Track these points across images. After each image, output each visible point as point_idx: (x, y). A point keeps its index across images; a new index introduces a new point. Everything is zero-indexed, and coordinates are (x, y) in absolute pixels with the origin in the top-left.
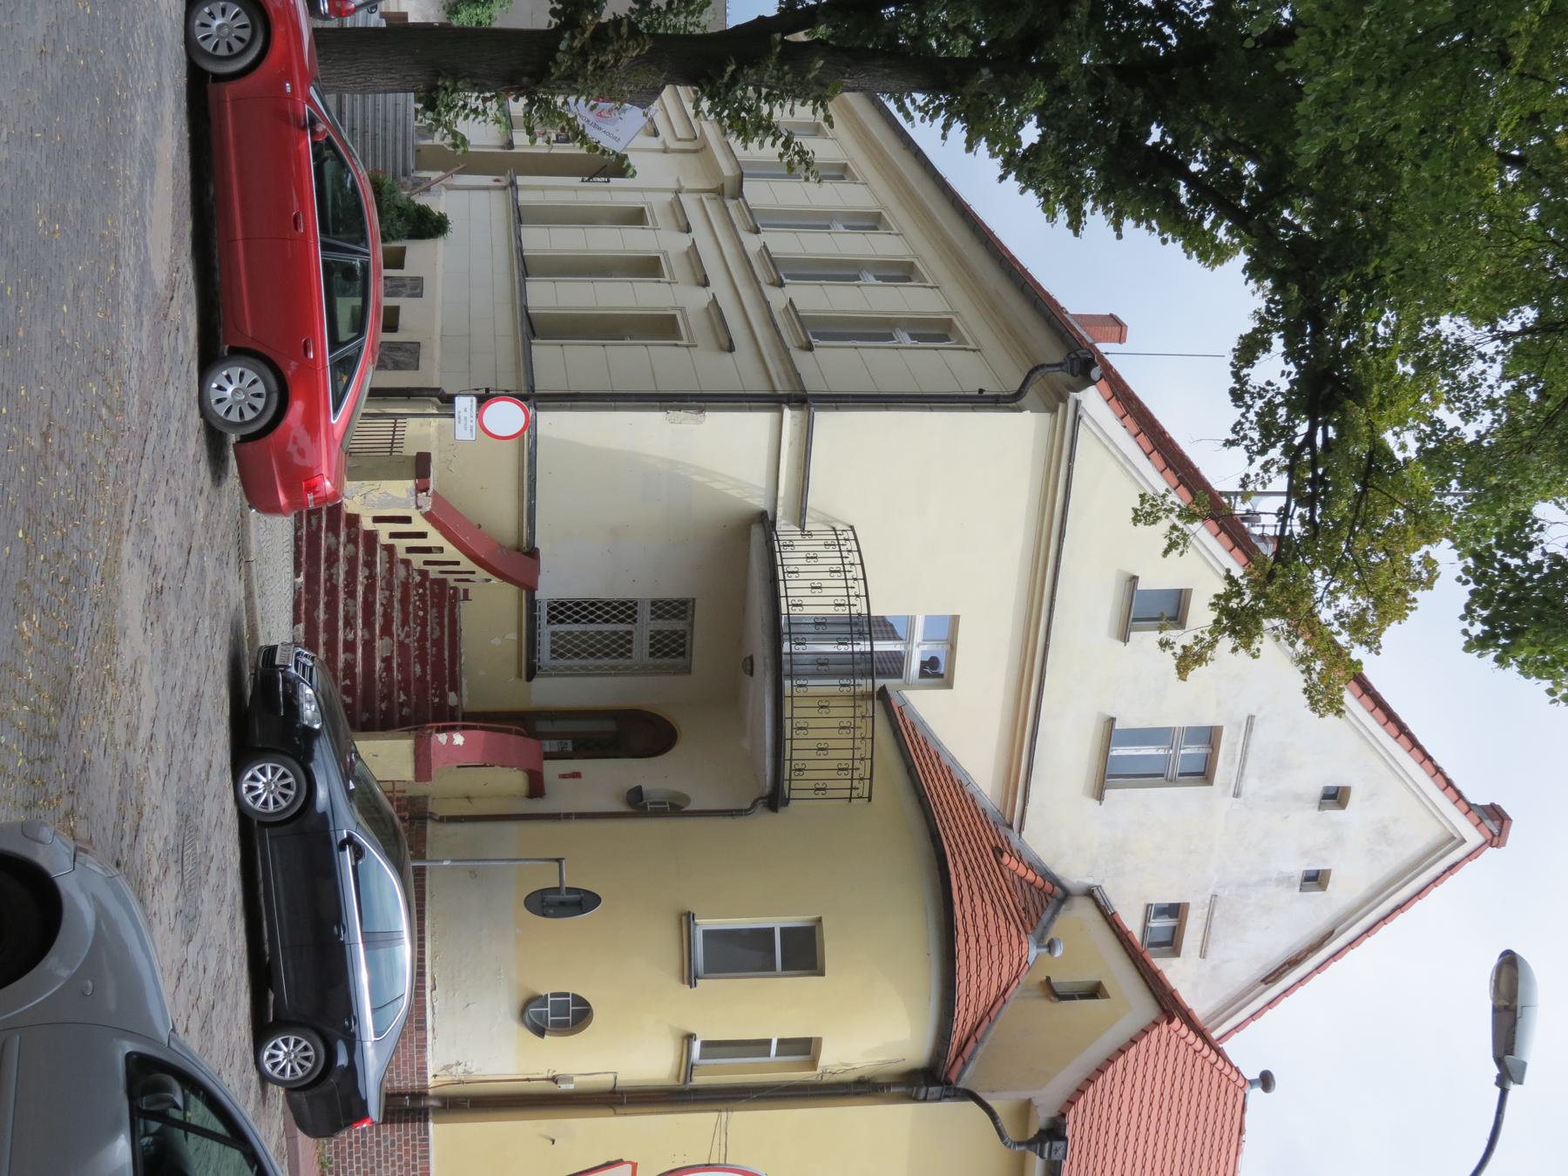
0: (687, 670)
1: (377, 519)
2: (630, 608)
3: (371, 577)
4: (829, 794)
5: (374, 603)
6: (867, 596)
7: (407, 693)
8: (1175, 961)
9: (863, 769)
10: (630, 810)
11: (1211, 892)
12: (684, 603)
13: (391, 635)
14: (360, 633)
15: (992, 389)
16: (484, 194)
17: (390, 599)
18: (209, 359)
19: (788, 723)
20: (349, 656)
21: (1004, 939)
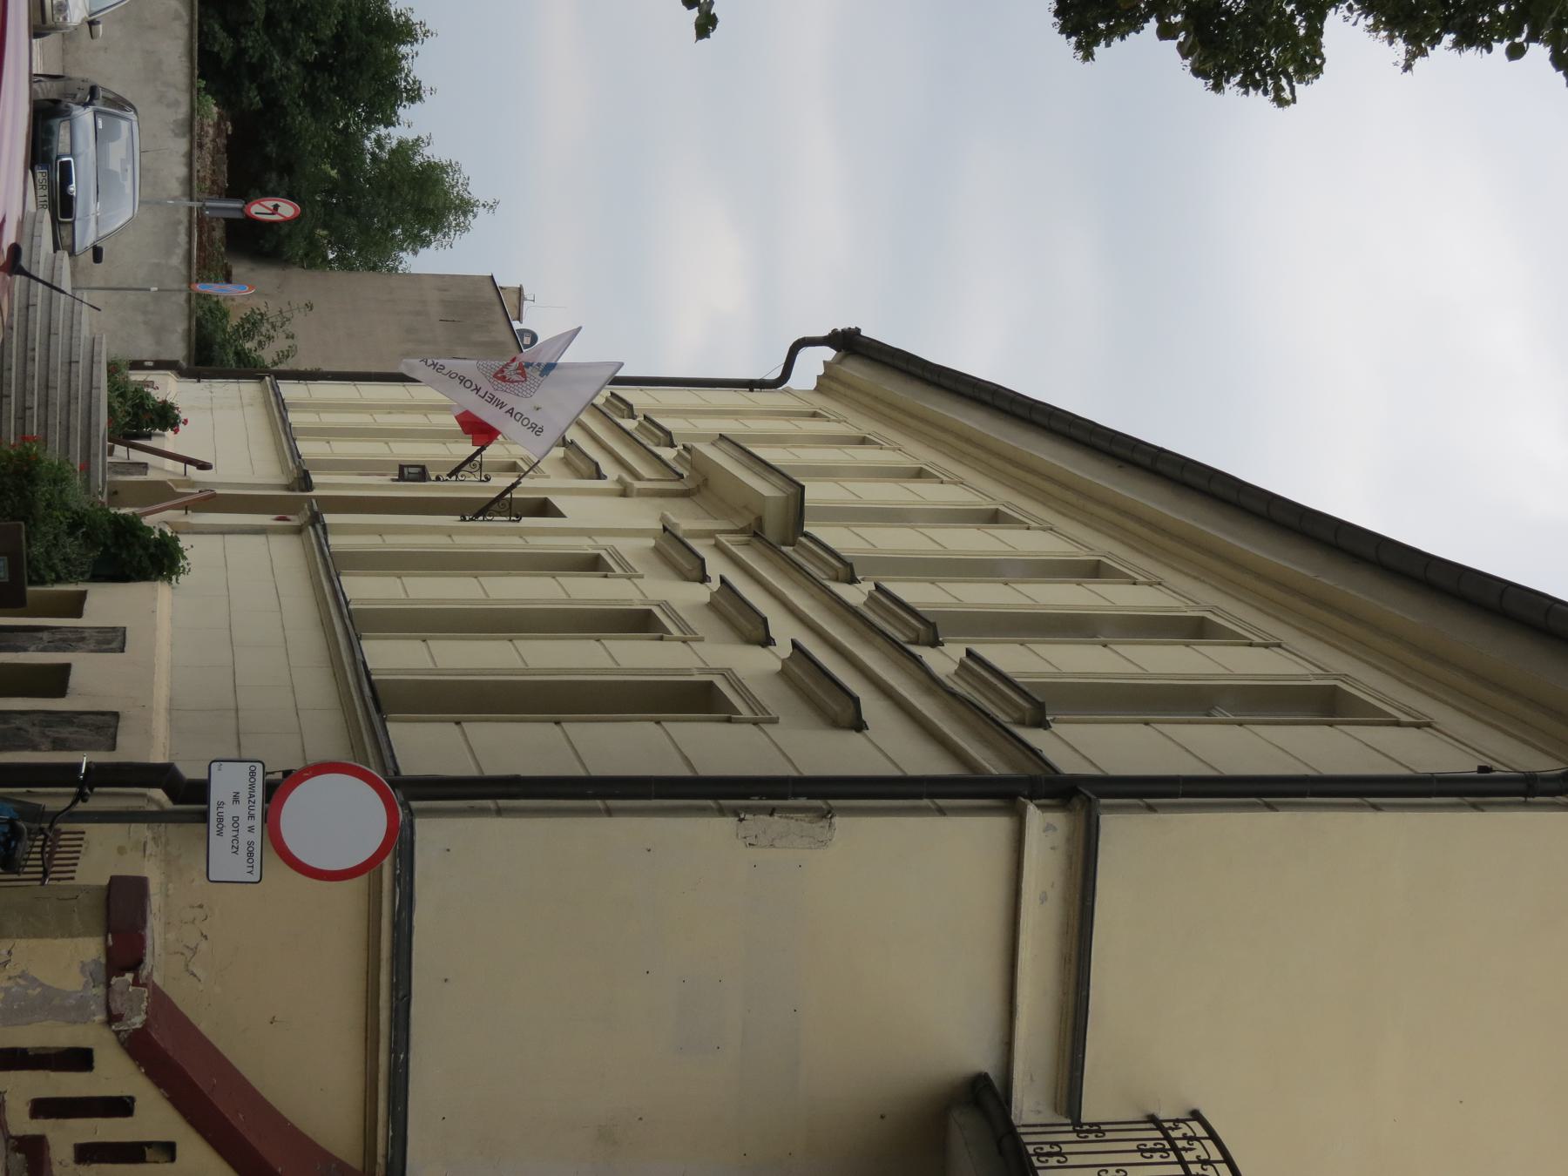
16: (260, 539)
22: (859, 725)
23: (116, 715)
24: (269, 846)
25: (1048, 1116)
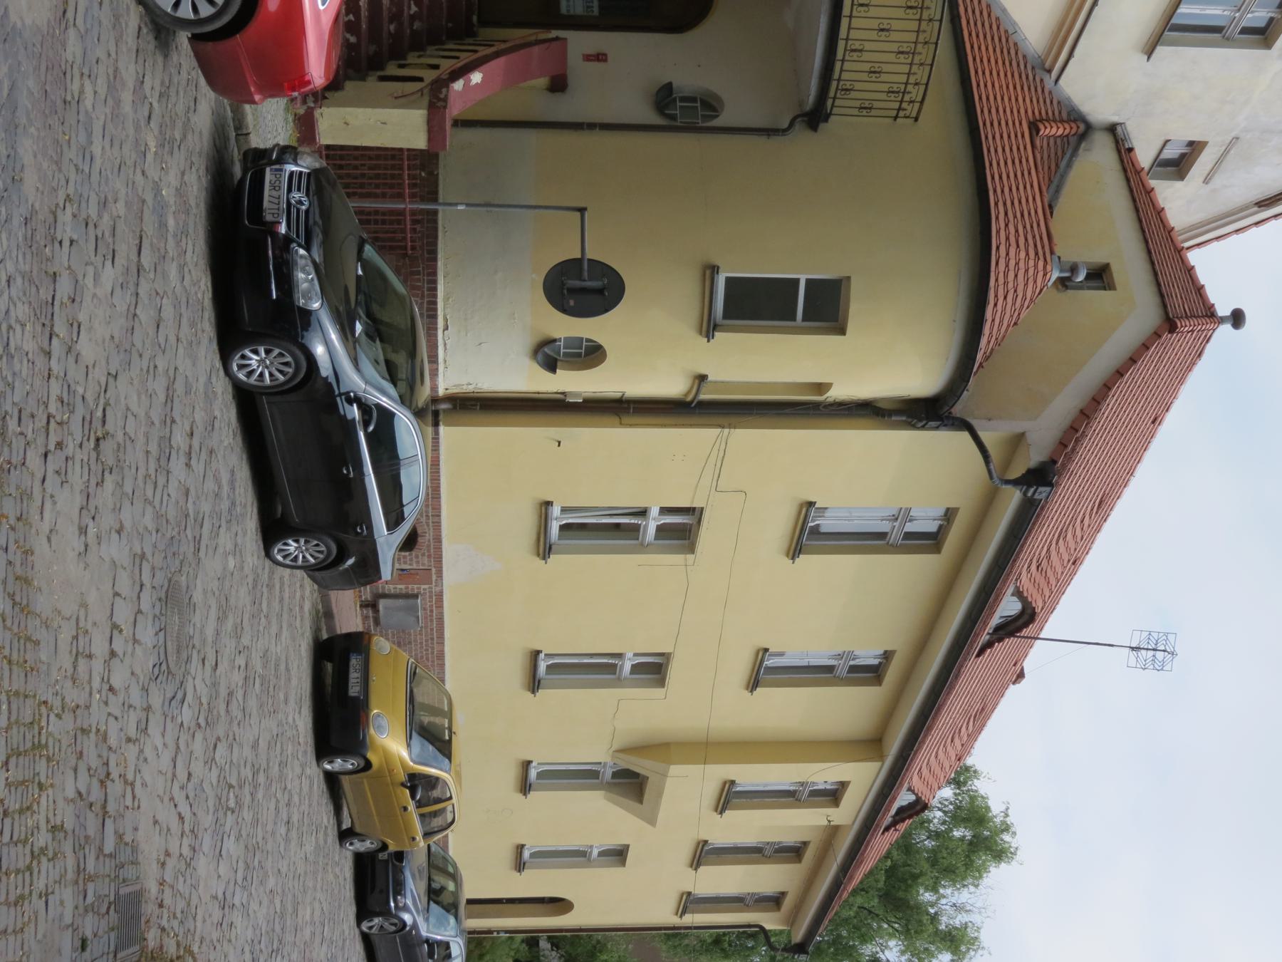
4: (873, 112)
9: (916, 93)
11: (1233, 134)
19: (841, 44)
21: (1031, 280)
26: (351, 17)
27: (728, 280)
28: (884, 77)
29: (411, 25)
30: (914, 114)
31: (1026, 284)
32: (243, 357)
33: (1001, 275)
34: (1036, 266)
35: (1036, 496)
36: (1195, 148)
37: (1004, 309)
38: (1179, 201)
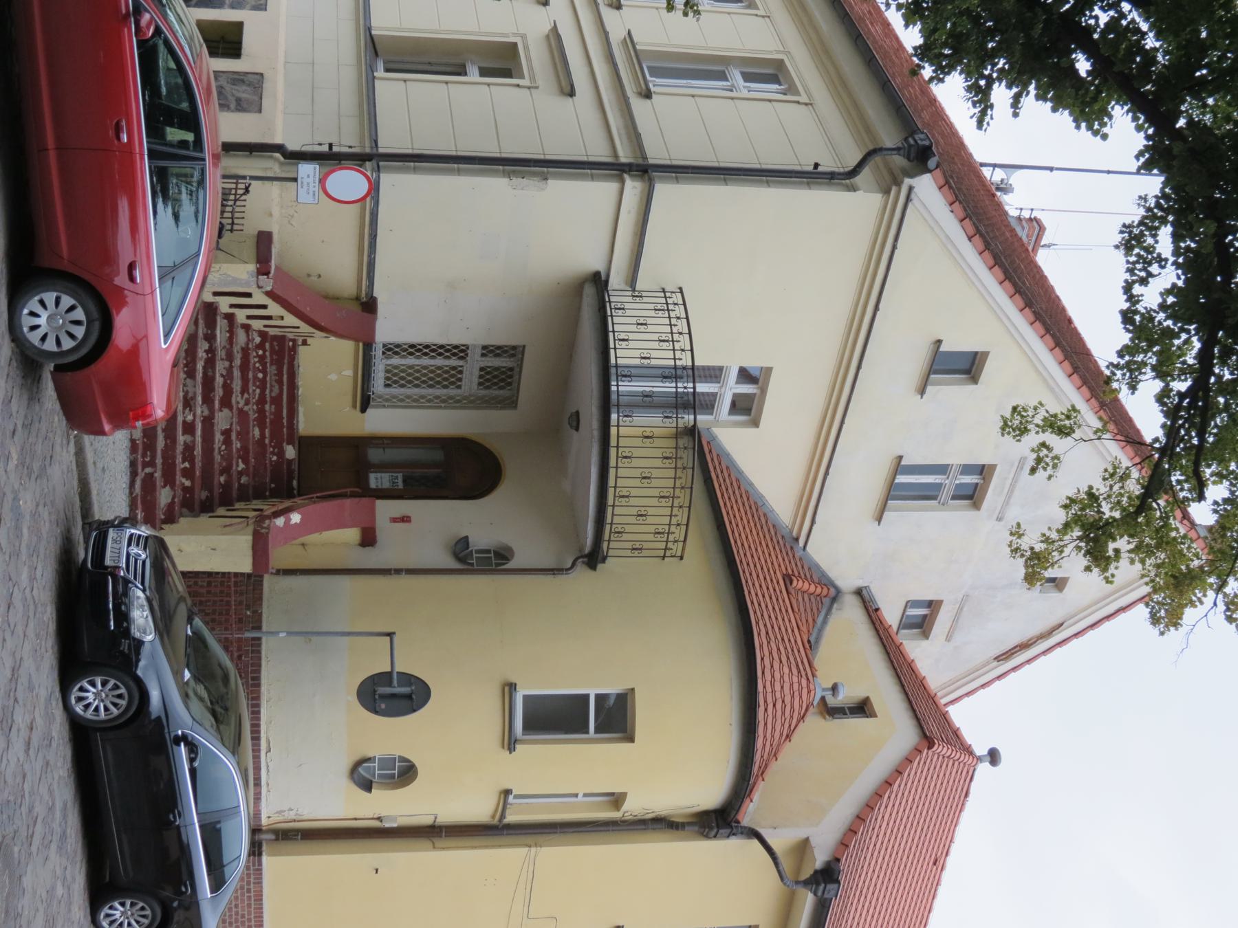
0: (512, 403)
1: (216, 294)
2: (462, 351)
3: (211, 351)
4: (645, 553)
5: (213, 378)
6: (692, 350)
7: (246, 462)
8: (924, 643)
10: (458, 566)
12: (514, 348)
13: (231, 408)
14: (199, 411)
15: (827, 165)
17: (230, 369)
18: (17, 292)
19: (611, 492)
20: (188, 438)
21: (796, 694)
22: (572, 94)
23: (260, 111)
24: (322, 193)
25: (623, 287)
26: (187, 465)
27: (526, 698)
28: (650, 520)
29: (239, 479)
30: (679, 554)
31: (793, 697)
32: (82, 689)
33: (768, 684)
34: (800, 683)
35: (826, 896)
36: (933, 606)
37: (775, 717)
38: (925, 655)
